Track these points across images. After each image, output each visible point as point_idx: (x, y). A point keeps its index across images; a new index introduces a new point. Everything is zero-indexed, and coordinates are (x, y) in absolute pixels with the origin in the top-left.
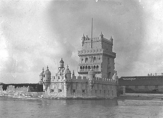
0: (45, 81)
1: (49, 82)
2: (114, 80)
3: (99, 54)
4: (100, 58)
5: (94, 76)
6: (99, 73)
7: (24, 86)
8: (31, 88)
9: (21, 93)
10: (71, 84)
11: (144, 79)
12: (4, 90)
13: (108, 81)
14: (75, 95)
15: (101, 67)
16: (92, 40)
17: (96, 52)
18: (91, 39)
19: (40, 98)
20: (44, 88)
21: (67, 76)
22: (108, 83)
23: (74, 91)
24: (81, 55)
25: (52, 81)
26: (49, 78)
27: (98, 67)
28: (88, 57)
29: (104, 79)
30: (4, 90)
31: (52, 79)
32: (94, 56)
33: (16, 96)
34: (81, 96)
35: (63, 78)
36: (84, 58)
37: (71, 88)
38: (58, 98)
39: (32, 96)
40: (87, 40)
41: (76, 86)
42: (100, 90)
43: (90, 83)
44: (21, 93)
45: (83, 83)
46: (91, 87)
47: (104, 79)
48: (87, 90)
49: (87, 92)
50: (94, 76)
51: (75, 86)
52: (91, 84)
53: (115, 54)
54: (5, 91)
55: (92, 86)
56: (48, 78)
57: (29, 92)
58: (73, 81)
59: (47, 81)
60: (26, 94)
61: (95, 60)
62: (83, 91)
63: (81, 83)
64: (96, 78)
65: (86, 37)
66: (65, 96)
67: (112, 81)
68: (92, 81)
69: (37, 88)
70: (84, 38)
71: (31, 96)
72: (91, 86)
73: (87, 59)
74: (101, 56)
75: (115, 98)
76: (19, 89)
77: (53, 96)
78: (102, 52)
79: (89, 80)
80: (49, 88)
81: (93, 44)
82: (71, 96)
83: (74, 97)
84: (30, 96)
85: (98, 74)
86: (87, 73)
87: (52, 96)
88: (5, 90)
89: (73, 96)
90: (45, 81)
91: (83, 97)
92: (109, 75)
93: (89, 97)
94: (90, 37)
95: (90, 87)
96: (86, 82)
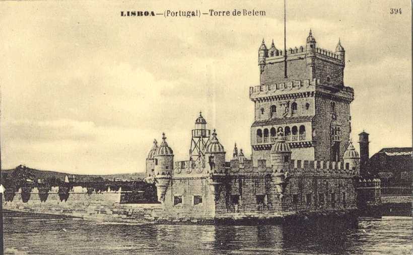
0: (158, 174)
1: (169, 176)
2: (348, 164)
3: (142, 12)
4: (307, 106)
5: (286, 157)
6: (307, 145)
7: (109, 189)
8: (126, 193)
9: (103, 207)
10: (227, 181)
11: (324, 59)
12: (62, 201)
13: (336, 167)
14: (238, 211)
15: (313, 129)
16: (286, 57)
17: (297, 87)
18: (283, 54)
19: (149, 220)
20: (159, 192)
21: (214, 160)
22: (336, 172)
23: (235, 200)
24: (261, 98)
25: (175, 176)
26: (169, 167)
27: (303, 129)
28: (274, 103)
29: (319, 162)
30: (62, 201)
31: (175, 170)
32: (292, 100)
33: (91, 214)
34: (255, 214)
35: (204, 167)
36: (267, 106)
37: (228, 194)
38: (193, 219)
39: (131, 215)
40: (272, 55)
41: (240, 185)
42: (309, 196)
43: (278, 176)
44: (103, 207)
45: (257, 178)
46: (279, 189)
47: (319, 162)
48: (269, 196)
49: (270, 202)
50: (286, 157)
51: (238, 187)
52: (279, 181)
53: (350, 90)
54: (64, 201)
55: (284, 185)
56: (167, 168)
57: (122, 205)
58: (232, 174)
59: (163, 174)
60: (115, 210)
61: (295, 111)
62: (260, 199)
63: (253, 178)
64: (296, 162)
65: (269, 46)
66: (213, 215)
67: (342, 168)
68: (282, 171)
69: (138, 190)
70: (266, 51)
71: (128, 216)
72: (280, 184)
73: (273, 108)
74: (312, 100)
75: (352, 212)
76: (96, 195)
77: (181, 216)
78: (312, 89)
79: (274, 169)
80: (169, 192)
81: (288, 66)
82: (228, 215)
83: (237, 216)
84: (125, 214)
85: (305, 149)
86: (269, 148)
87: (178, 214)
88: (66, 200)
89: (232, 214)
90: (160, 176)
91: (261, 216)
92: (336, 150)
93: (276, 215)
94: (280, 47)
95: (278, 186)
96: (265, 174)
